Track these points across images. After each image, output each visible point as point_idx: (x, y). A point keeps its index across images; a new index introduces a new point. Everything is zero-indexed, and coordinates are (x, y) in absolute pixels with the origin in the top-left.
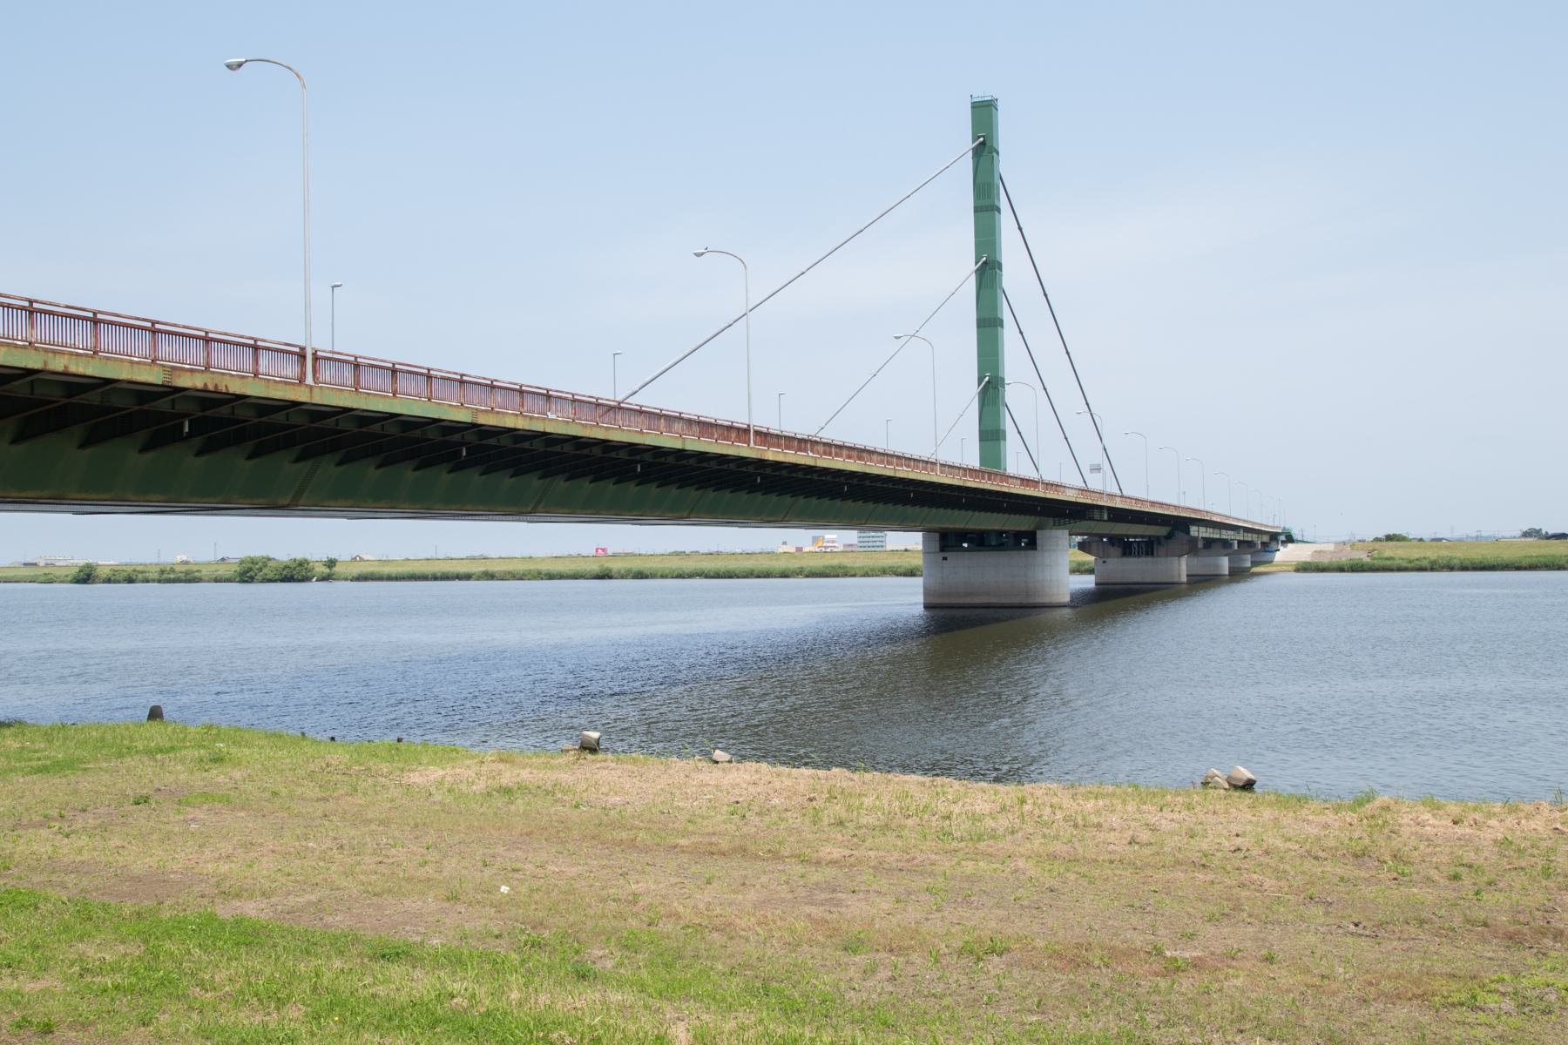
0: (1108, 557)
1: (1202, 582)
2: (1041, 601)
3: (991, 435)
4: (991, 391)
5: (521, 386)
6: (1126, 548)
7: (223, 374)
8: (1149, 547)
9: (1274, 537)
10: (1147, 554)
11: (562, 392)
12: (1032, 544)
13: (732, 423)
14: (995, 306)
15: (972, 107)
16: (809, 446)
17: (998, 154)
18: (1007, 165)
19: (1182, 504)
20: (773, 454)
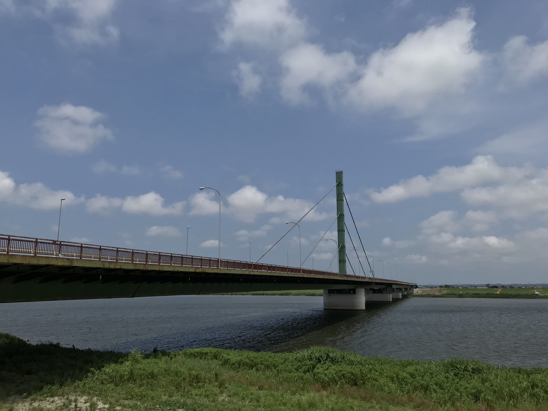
0: (369, 293)
1: (396, 301)
2: (358, 309)
3: (342, 261)
4: (342, 249)
5: (182, 256)
6: (375, 291)
7: (49, 257)
8: (380, 291)
9: (412, 286)
10: (380, 293)
11: (93, 245)
12: (354, 292)
13: (262, 264)
14: (343, 226)
15: (336, 173)
16: (284, 269)
17: (343, 185)
18: (345, 189)
19: (385, 279)
20: (306, 276)
